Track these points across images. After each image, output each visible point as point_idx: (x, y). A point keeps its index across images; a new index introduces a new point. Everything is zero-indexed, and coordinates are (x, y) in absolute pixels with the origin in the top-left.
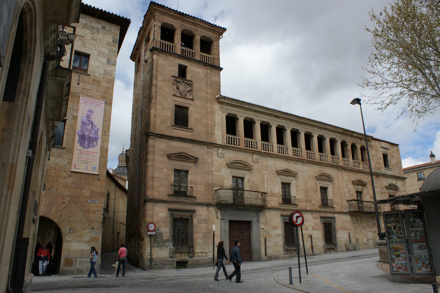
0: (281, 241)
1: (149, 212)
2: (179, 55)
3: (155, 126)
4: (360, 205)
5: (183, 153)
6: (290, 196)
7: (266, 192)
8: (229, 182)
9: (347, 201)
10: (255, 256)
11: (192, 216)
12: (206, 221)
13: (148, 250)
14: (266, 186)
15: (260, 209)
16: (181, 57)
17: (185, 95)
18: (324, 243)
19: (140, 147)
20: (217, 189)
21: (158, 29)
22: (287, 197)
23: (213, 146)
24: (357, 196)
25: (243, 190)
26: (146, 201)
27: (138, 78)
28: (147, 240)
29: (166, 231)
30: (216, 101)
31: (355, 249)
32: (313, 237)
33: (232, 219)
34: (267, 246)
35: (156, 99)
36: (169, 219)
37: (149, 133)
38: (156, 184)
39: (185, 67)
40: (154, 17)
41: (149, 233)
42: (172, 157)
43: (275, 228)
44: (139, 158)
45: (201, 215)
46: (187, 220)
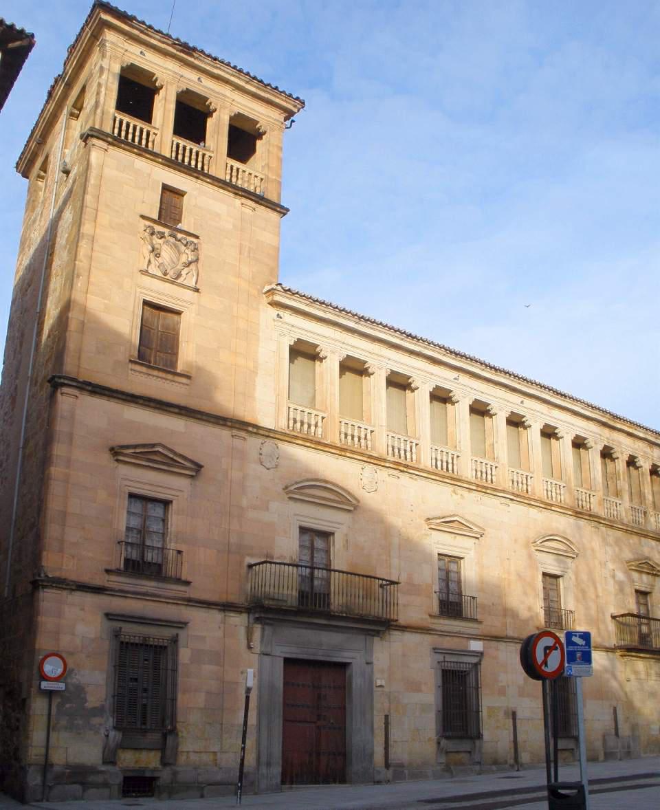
0: (429, 724)
1: (46, 621)
2: (164, 158)
3: (79, 358)
4: (645, 629)
5: (160, 445)
6: (460, 594)
7: (394, 579)
8: (288, 546)
9: (614, 617)
10: (356, 767)
11: (175, 640)
12: (218, 657)
13: (37, 736)
14: (395, 562)
15: (380, 625)
16: (172, 164)
17: (179, 275)
19: (27, 421)
20: (253, 561)
21: (111, 80)
22: (452, 598)
23: (248, 432)
24: (638, 603)
25: (330, 570)
26: (36, 585)
27: (34, 222)
28: (38, 706)
29: (96, 681)
30: (265, 300)
31: (628, 754)
32: (519, 715)
33: (294, 656)
34: (392, 738)
36: (107, 645)
37: (60, 377)
38: (73, 535)
39: (180, 194)
40: (103, 45)
41: (44, 685)
42: (126, 455)
43: (415, 687)
44: (23, 457)
46: (159, 650)
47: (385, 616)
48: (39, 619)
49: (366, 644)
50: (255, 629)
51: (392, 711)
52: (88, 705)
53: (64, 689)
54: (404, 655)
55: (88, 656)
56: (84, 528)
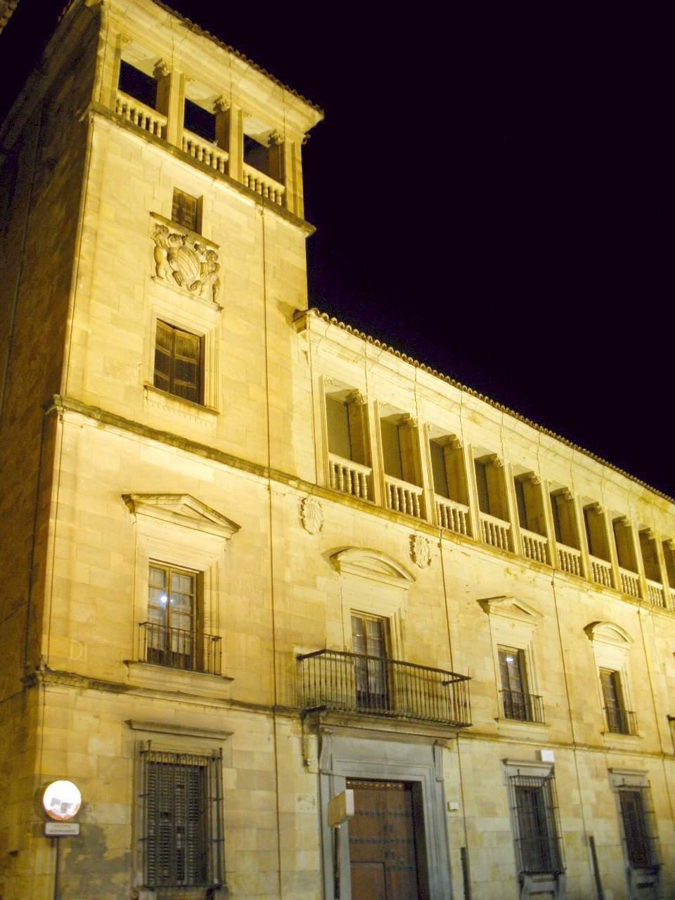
7: (466, 674)
11: (216, 758)
18: (628, 864)
32: (597, 842)
35: (92, 279)
38: (81, 614)
45: (248, 755)
47: (462, 721)
48: (39, 730)
49: (665, 777)
50: (310, 740)
51: (469, 844)
52: (109, 856)
53: (77, 833)
54: (475, 770)
55: (107, 783)
56: (95, 604)
